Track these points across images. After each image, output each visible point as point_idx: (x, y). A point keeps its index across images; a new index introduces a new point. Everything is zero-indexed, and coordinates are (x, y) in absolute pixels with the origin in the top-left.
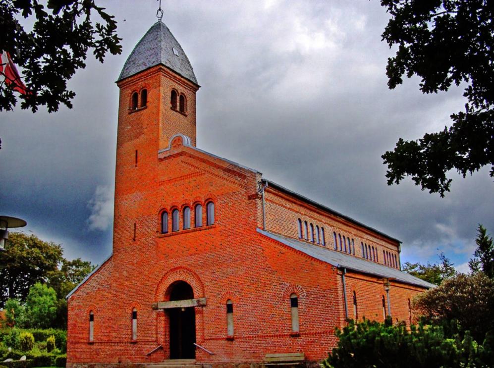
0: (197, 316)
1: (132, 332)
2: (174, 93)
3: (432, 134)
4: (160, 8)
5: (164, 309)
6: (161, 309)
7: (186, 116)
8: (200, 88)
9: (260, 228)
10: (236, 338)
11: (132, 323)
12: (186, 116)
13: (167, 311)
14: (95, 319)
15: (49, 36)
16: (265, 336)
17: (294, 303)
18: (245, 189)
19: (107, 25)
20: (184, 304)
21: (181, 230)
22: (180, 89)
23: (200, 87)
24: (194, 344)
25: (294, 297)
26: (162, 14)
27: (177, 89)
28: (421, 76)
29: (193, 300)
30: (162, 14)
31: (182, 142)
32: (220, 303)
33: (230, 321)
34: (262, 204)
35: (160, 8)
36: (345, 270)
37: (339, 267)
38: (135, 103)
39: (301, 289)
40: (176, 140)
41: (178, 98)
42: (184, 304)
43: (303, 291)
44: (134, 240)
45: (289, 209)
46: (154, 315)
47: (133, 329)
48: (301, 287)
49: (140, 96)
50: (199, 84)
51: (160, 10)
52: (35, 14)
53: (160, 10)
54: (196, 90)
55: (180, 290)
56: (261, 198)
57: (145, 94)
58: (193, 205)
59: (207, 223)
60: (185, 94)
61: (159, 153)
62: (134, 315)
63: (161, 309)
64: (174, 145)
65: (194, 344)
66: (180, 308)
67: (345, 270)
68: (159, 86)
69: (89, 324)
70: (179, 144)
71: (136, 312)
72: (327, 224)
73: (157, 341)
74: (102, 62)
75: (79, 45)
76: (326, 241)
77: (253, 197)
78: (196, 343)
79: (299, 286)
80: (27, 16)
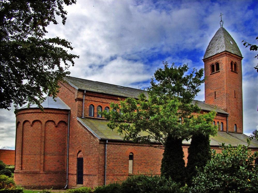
3: (60, 64)
4: (221, 20)
7: (237, 73)
8: (243, 58)
12: (237, 73)
15: (253, 48)
19: (2, 177)
22: (234, 60)
23: (243, 58)
30: (223, 23)
35: (221, 20)
38: (213, 70)
50: (243, 57)
51: (221, 21)
52: (191, 141)
53: (221, 21)
54: (241, 59)
55: (215, 98)
74: (48, 32)
75: (34, 57)
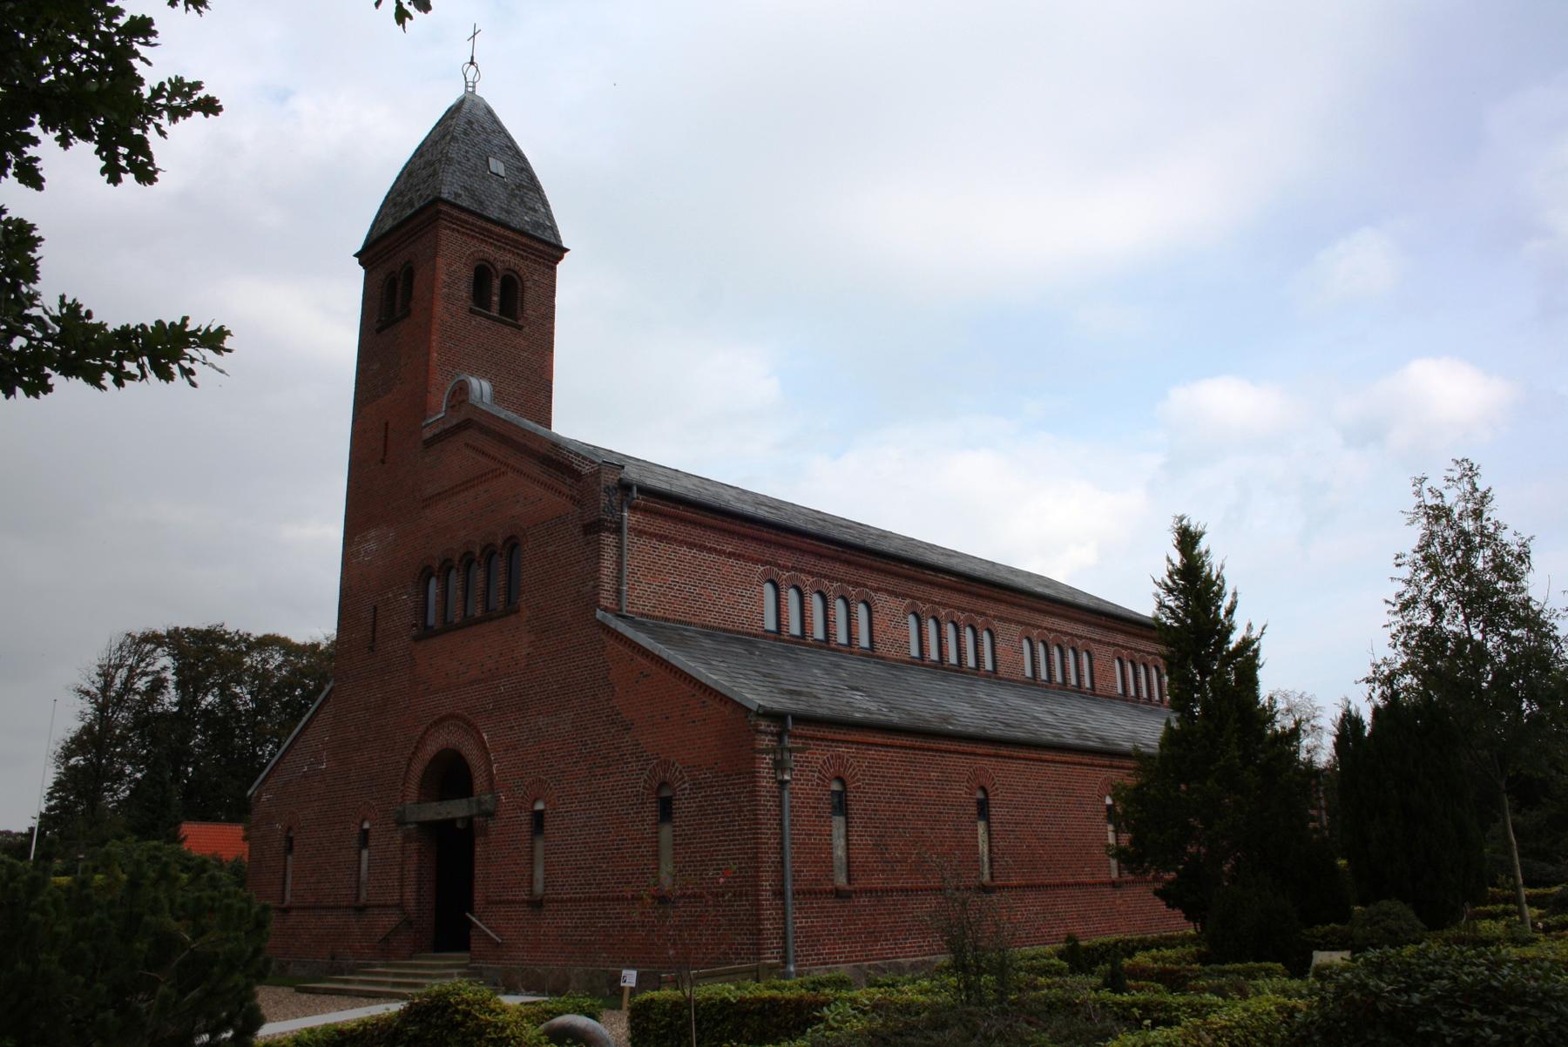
0: (479, 840)
1: (358, 881)
2: (482, 275)
4: (472, 58)
5: (416, 823)
6: (411, 823)
9: (606, 609)
10: (549, 901)
11: (360, 857)
13: (425, 826)
14: (372, 843)
16: (603, 900)
17: (666, 810)
18: (580, 508)
20: (457, 809)
21: (457, 620)
22: (504, 259)
24: (468, 914)
25: (666, 793)
26: (477, 68)
27: (492, 259)
28: (139, 76)
29: (471, 799)
31: (467, 394)
32: (521, 808)
33: (539, 853)
34: (620, 547)
36: (790, 718)
37: (760, 712)
39: (680, 772)
40: (456, 391)
41: (497, 283)
42: (457, 809)
43: (683, 777)
44: (371, 649)
45: (730, 555)
46: (399, 836)
47: (843, 831)
48: (680, 767)
49: (400, 285)
51: (472, 63)
53: (472, 63)
56: (618, 530)
57: (409, 274)
58: (481, 554)
59: (509, 601)
60: (521, 273)
61: (425, 427)
62: (364, 838)
63: (411, 823)
64: (453, 403)
65: (468, 914)
66: (453, 821)
67: (790, 718)
68: (436, 254)
69: (286, 859)
70: (460, 399)
71: (366, 832)
72: (887, 591)
73: (400, 906)
76: (876, 639)
77: (593, 528)
78: (472, 914)
79: (677, 765)
80: (221, 106)
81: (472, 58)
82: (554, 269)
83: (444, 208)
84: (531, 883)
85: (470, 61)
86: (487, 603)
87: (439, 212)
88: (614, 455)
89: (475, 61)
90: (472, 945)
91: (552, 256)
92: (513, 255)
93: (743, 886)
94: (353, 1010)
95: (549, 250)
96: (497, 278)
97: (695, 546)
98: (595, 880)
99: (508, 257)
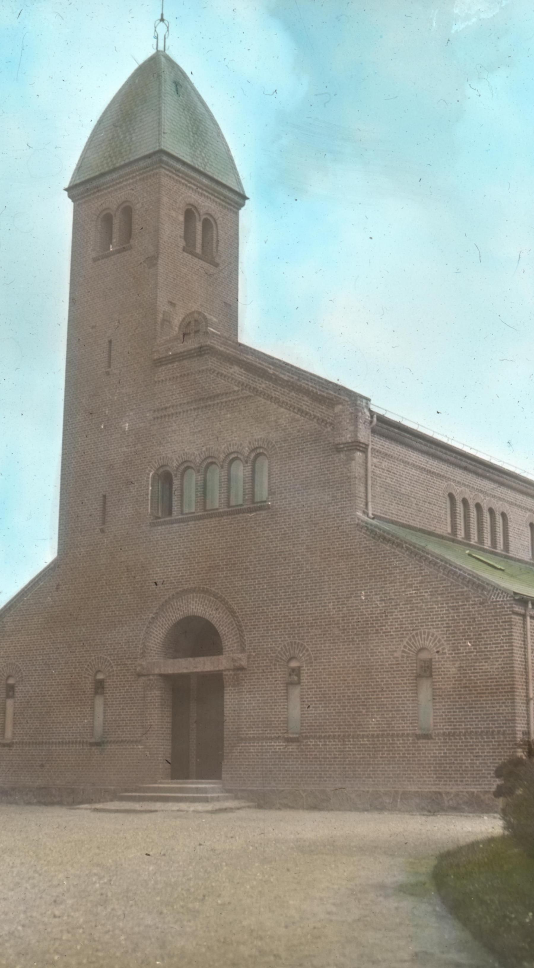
4: (162, 15)
13: (165, 677)
51: (162, 20)
53: (162, 20)
81: (162, 15)
82: (237, 214)
83: (165, 158)
84: (105, 704)
85: (160, 17)
86: (205, 503)
87: (161, 161)
88: (331, 385)
89: (165, 18)
90: (223, 776)
91: (237, 203)
92: (216, 204)
93: (317, 732)
94: (113, 803)
95: (236, 198)
96: (200, 220)
97: (425, 471)
98: (120, 701)
99: (208, 203)
